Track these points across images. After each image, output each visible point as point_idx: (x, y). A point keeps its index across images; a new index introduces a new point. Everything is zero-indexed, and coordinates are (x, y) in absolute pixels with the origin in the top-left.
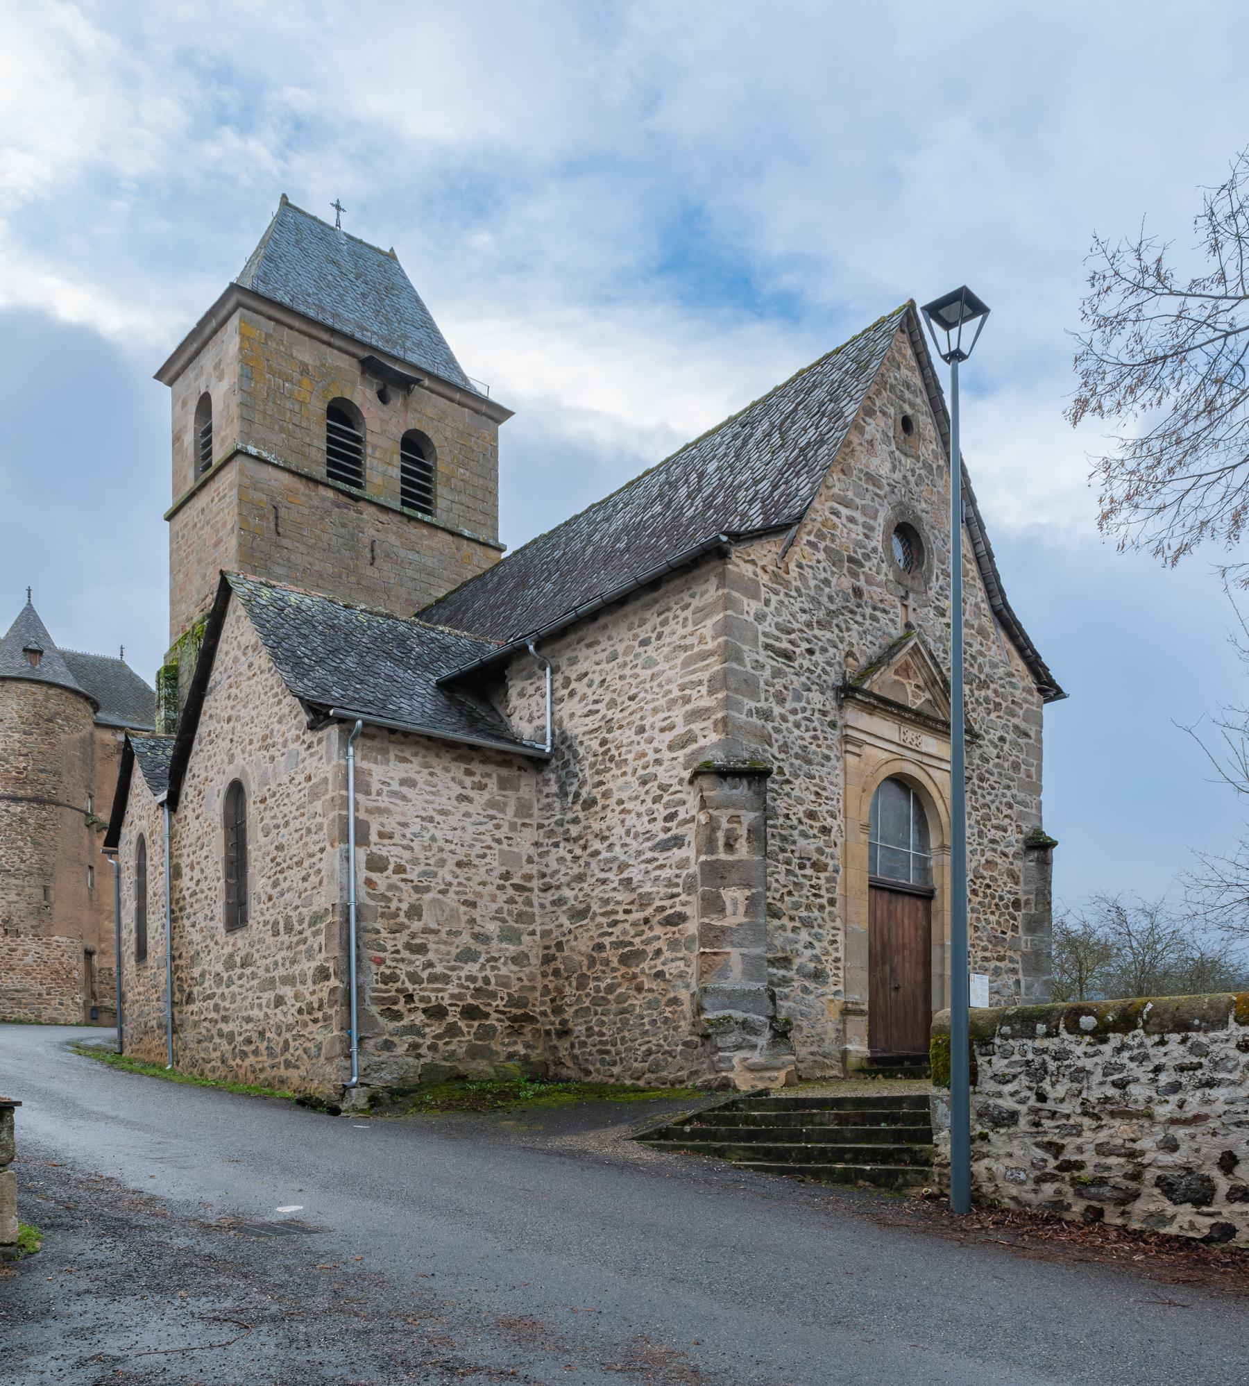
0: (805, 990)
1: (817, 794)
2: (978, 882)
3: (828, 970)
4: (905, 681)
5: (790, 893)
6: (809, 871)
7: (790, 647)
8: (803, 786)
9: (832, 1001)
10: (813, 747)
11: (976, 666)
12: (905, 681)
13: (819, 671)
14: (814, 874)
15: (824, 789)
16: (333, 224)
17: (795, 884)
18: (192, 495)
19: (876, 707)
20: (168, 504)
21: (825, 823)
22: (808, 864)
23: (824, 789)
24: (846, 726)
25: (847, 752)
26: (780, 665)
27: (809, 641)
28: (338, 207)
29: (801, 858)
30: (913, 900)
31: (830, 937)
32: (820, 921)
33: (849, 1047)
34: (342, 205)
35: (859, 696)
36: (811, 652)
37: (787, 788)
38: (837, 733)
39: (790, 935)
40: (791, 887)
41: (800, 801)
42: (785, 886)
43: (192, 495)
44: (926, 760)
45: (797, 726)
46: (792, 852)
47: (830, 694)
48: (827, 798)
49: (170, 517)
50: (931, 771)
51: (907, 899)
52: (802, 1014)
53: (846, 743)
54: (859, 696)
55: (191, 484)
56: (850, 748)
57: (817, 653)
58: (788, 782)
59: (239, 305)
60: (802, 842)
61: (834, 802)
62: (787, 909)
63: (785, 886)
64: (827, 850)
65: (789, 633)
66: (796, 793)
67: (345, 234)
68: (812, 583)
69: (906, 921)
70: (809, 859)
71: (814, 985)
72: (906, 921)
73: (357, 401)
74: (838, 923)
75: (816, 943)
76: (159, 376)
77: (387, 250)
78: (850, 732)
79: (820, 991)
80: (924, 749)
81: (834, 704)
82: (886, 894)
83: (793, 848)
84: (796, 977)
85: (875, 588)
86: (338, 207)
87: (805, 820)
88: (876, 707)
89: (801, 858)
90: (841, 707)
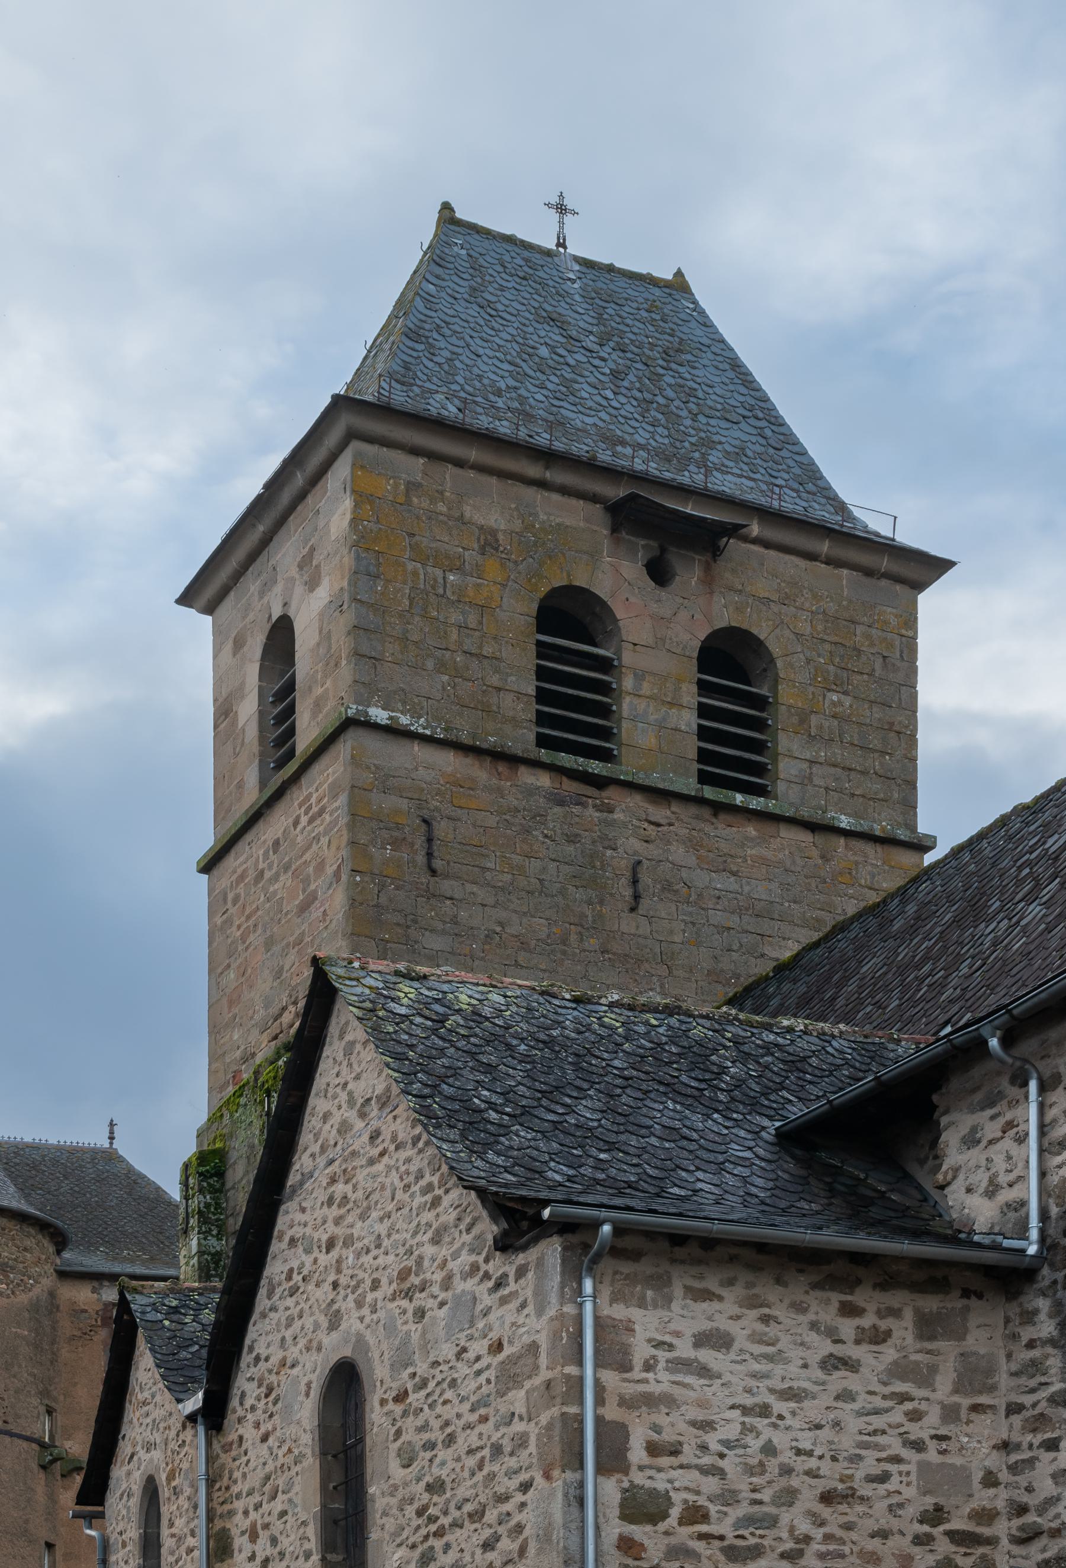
16: (551, 244)
18: (254, 818)
20: (206, 841)
28: (561, 209)
34: (569, 203)
43: (254, 818)
49: (209, 865)
55: (251, 796)
59: (352, 435)
67: (577, 259)
76: (186, 599)
77: (669, 276)
86: (561, 209)
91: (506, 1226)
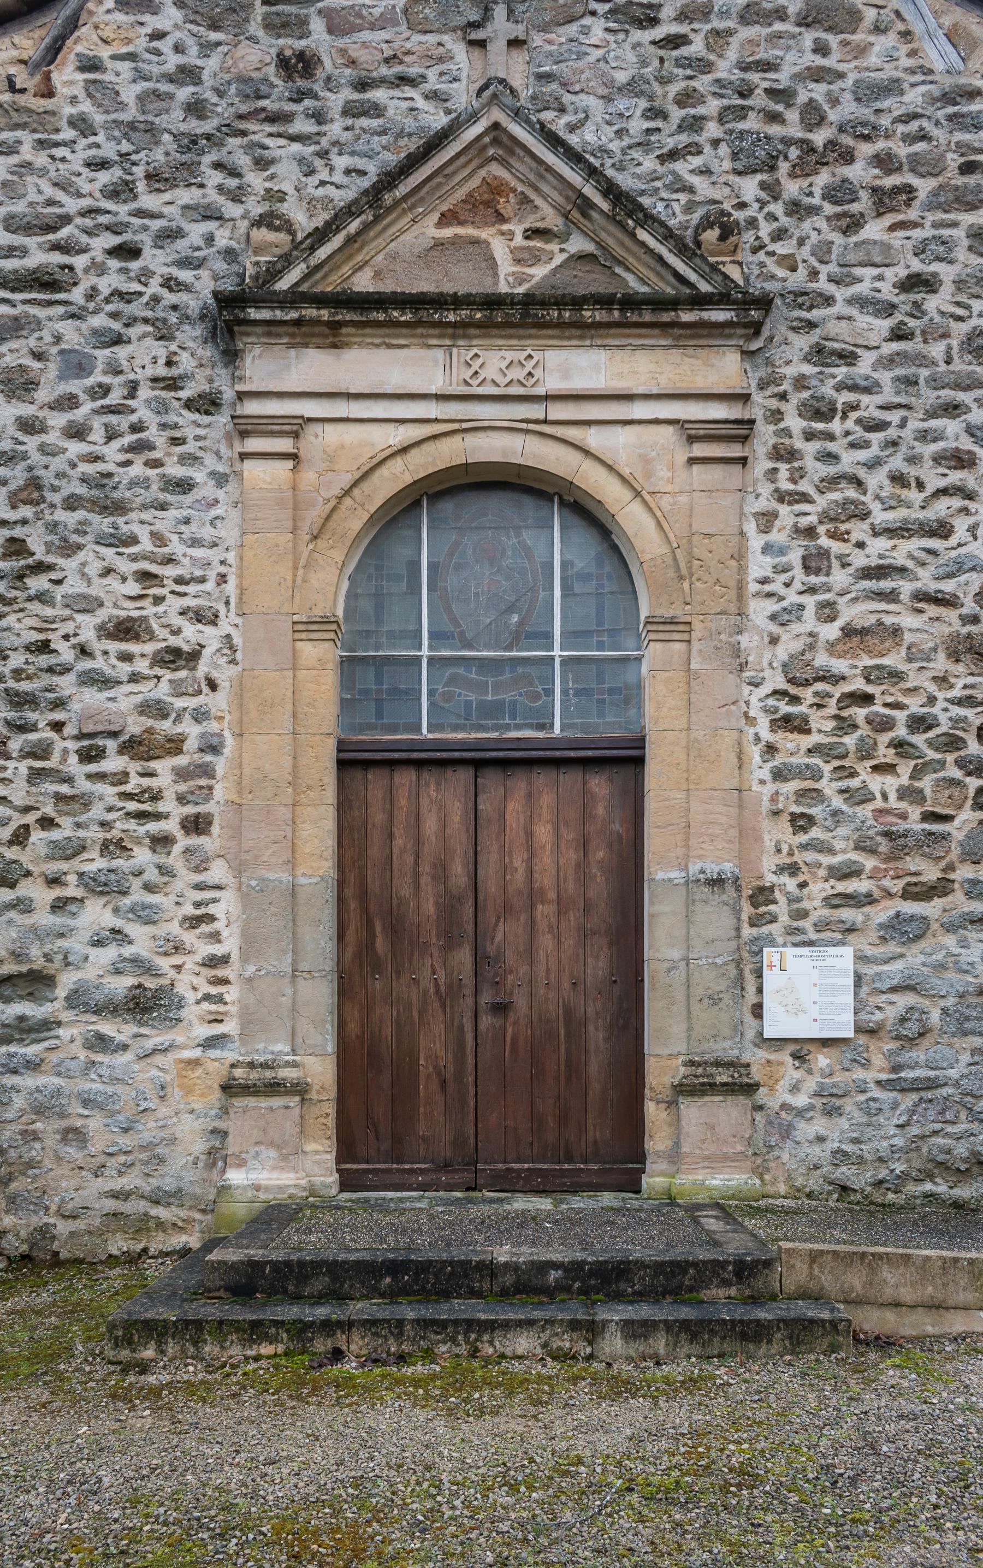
0: (100, 1042)
1: (145, 577)
2: (808, 694)
3: (182, 989)
4: (484, 234)
5: (47, 823)
6: (113, 763)
7: (57, 258)
8: (94, 568)
9: (196, 1063)
10: (137, 469)
11: (793, 116)
12: (484, 234)
13: (154, 287)
14: (134, 767)
15: (169, 560)
17: (60, 798)
19: (335, 326)
21: (174, 641)
22: (111, 745)
23: (169, 560)
24: (241, 396)
25: (243, 456)
26: (20, 309)
27: (114, 229)
29: (81, 736)
30: (570, 779)
31: (189, 910)
32: (152, 875)
33: (235, 1177)
35: (253, 314)
36: (128, 252)
37: (37, 583)
38: (222, 420)
39: (44, 919)
40: (48, 809)
41: (88, 604)
42: (27, 809)
44: (559, 412)
45: (77, 432)
46: (57, 726)
47: (190, 334)
48: (180, 581)
50: (593, 438)
51: (542, 779)
52: (86, 1103)
53: (244, 434)
54: (253, 314)
56: (255, 444)
57: (148, 251)
58: (40, 568)
60: (92, 697)
61: (210, 586)
62: (36, 860)
63: (27, 809)
64: (179, 703)
65: (50, 228)
66: (74, 585)
68: (129, 93)
69: (543, 833)
70: (114, 735)
71: (132, 1029)
72: (543, 833)
73: (909, 181)
74: (218, 872)
75: (134, 930)
78: (252, 408)
79: (149, 1044)
80: (553, 384)
81: (207, 352)
82: (463, 776)
83: (59, 716)
84: (65, 1016)
85: (366, 35)
87: (97, 646)
88: (335, 326)
89: (81, 736)
90: (231, 356)
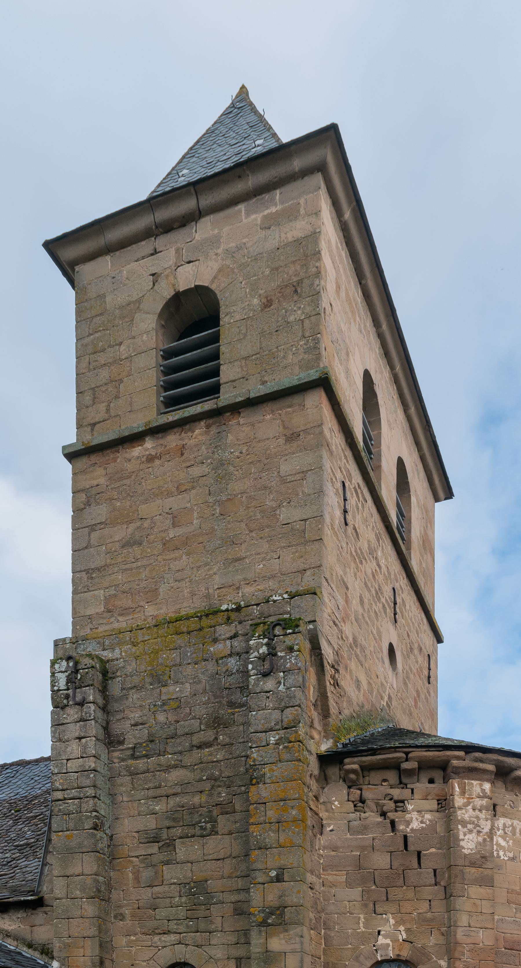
91: (466, 852)
